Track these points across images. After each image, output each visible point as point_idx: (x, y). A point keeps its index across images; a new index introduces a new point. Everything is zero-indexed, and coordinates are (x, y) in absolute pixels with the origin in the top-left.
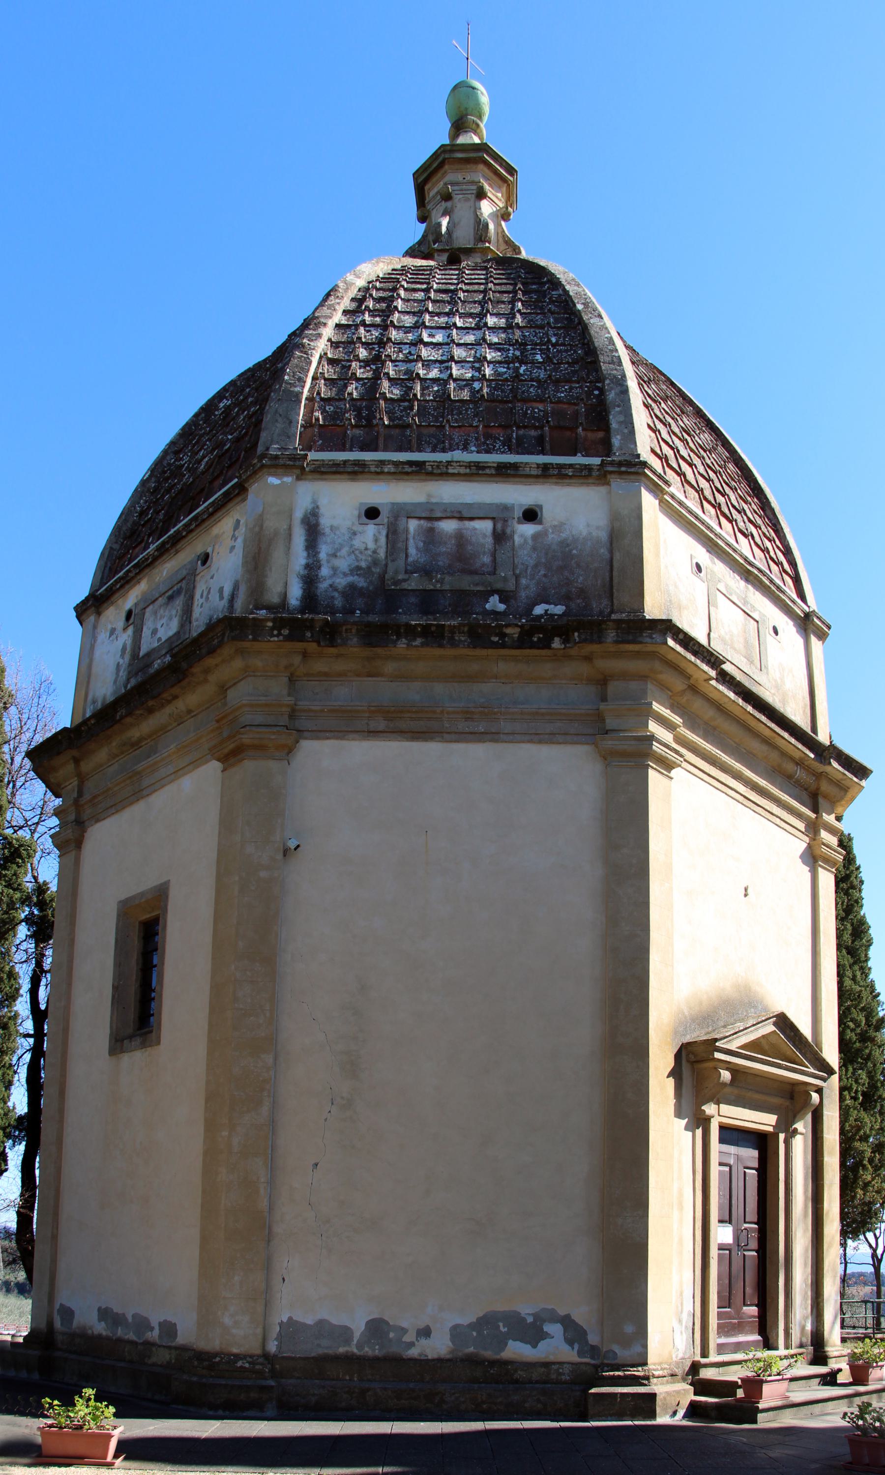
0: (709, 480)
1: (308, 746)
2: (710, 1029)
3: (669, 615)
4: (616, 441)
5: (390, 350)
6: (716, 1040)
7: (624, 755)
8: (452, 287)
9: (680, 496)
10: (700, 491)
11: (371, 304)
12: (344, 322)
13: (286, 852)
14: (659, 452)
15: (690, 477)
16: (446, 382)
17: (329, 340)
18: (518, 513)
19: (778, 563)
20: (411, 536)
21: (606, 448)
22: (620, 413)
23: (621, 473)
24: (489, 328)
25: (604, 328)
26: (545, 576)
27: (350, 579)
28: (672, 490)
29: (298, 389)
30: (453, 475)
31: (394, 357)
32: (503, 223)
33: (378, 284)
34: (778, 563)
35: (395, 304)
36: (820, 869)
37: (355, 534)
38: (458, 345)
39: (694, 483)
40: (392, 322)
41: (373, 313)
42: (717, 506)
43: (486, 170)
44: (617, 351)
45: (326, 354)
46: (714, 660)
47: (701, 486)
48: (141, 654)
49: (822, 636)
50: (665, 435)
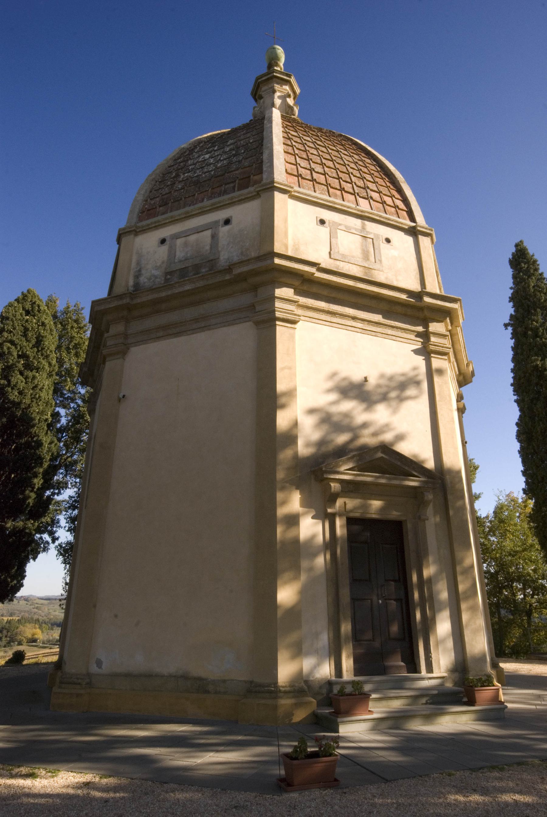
7: (264, 322)
13: (120, 400)
18: (222, 223)
20: (177, 247)
43: (277, 80)
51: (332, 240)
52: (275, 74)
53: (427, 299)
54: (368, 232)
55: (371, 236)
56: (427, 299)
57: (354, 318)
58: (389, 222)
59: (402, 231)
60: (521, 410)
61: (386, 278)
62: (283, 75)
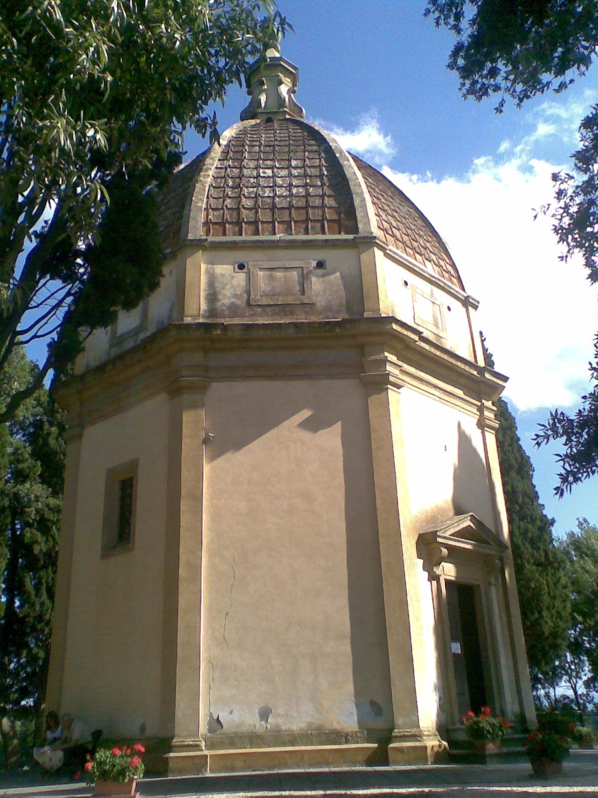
0: (408, 235)
1: (214, 385)
2: (434, 525)
3: (393, 312)
4: (360, 226)
5: (244, 181)
6: (437, 531)
8: (272, 144)
9: (394, 249)
10: (404, 243)
11: (231, 154)
12: (219, 166)
14: (382, 227)
15: (398, 236)
16: (273, 198)
17: (213, 176)
19: (448, 272)
21: (355, 230)
22: (361, 211)
23: (364, 243)
24: (293, 168)
25: (350, 166)
26: (329, 295)
27: (232, 300)
28: (390, 247)
29: (200, 204)
30: (280, 246)
31: (246, 185)
32: (292, 95)
33: (233, 142)
34: (448, 272)
35: (244, 155)
36: (486, 432)
37: (233, 277)
38: (278, 177)
39: (401, 239)
40: (244, 166)
41: (234, 160)
42: (413, 249)
44: (358, 179)
45: (212, 184)
46: (419, 333)
47: (405, 240)
48: (117, 335)
49: (476, 307)
50: (384, 217)
51: (415, 304)
52: (281, 62)
53: (487, 376)
54: (435, 300)
55: (439, 303)
56: (487, 376)
57: (436, 387)
58: (449, 289)
59: (459, 301)
60: (372, 395)
61: (451, 347)
62: (289, 66)
